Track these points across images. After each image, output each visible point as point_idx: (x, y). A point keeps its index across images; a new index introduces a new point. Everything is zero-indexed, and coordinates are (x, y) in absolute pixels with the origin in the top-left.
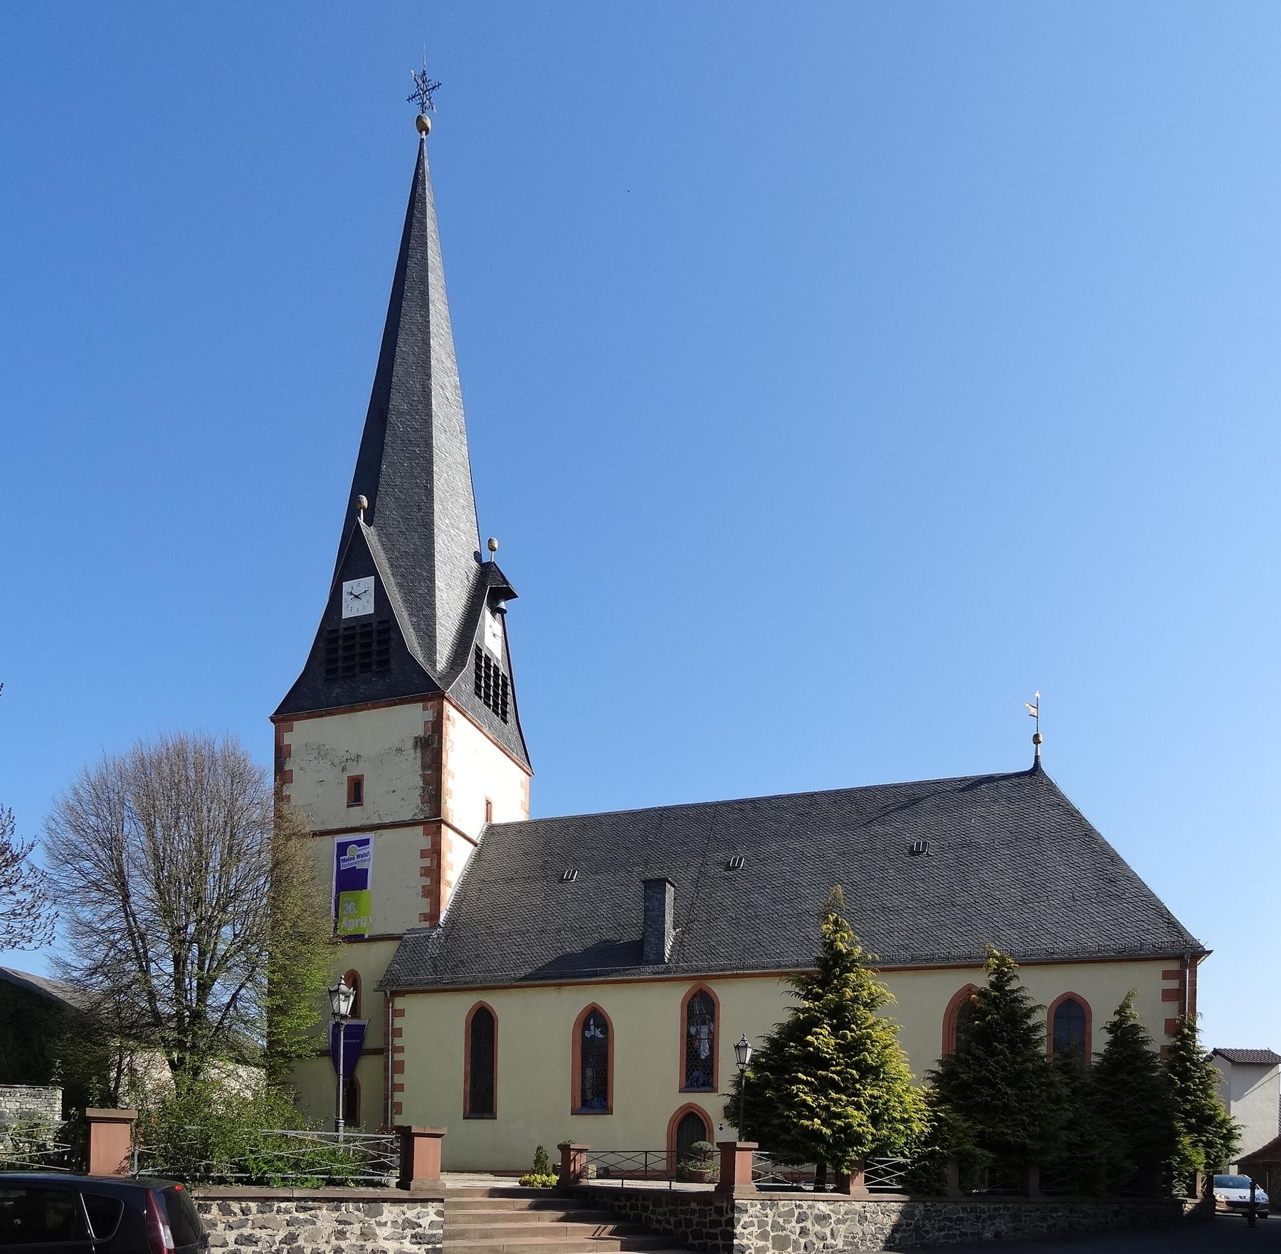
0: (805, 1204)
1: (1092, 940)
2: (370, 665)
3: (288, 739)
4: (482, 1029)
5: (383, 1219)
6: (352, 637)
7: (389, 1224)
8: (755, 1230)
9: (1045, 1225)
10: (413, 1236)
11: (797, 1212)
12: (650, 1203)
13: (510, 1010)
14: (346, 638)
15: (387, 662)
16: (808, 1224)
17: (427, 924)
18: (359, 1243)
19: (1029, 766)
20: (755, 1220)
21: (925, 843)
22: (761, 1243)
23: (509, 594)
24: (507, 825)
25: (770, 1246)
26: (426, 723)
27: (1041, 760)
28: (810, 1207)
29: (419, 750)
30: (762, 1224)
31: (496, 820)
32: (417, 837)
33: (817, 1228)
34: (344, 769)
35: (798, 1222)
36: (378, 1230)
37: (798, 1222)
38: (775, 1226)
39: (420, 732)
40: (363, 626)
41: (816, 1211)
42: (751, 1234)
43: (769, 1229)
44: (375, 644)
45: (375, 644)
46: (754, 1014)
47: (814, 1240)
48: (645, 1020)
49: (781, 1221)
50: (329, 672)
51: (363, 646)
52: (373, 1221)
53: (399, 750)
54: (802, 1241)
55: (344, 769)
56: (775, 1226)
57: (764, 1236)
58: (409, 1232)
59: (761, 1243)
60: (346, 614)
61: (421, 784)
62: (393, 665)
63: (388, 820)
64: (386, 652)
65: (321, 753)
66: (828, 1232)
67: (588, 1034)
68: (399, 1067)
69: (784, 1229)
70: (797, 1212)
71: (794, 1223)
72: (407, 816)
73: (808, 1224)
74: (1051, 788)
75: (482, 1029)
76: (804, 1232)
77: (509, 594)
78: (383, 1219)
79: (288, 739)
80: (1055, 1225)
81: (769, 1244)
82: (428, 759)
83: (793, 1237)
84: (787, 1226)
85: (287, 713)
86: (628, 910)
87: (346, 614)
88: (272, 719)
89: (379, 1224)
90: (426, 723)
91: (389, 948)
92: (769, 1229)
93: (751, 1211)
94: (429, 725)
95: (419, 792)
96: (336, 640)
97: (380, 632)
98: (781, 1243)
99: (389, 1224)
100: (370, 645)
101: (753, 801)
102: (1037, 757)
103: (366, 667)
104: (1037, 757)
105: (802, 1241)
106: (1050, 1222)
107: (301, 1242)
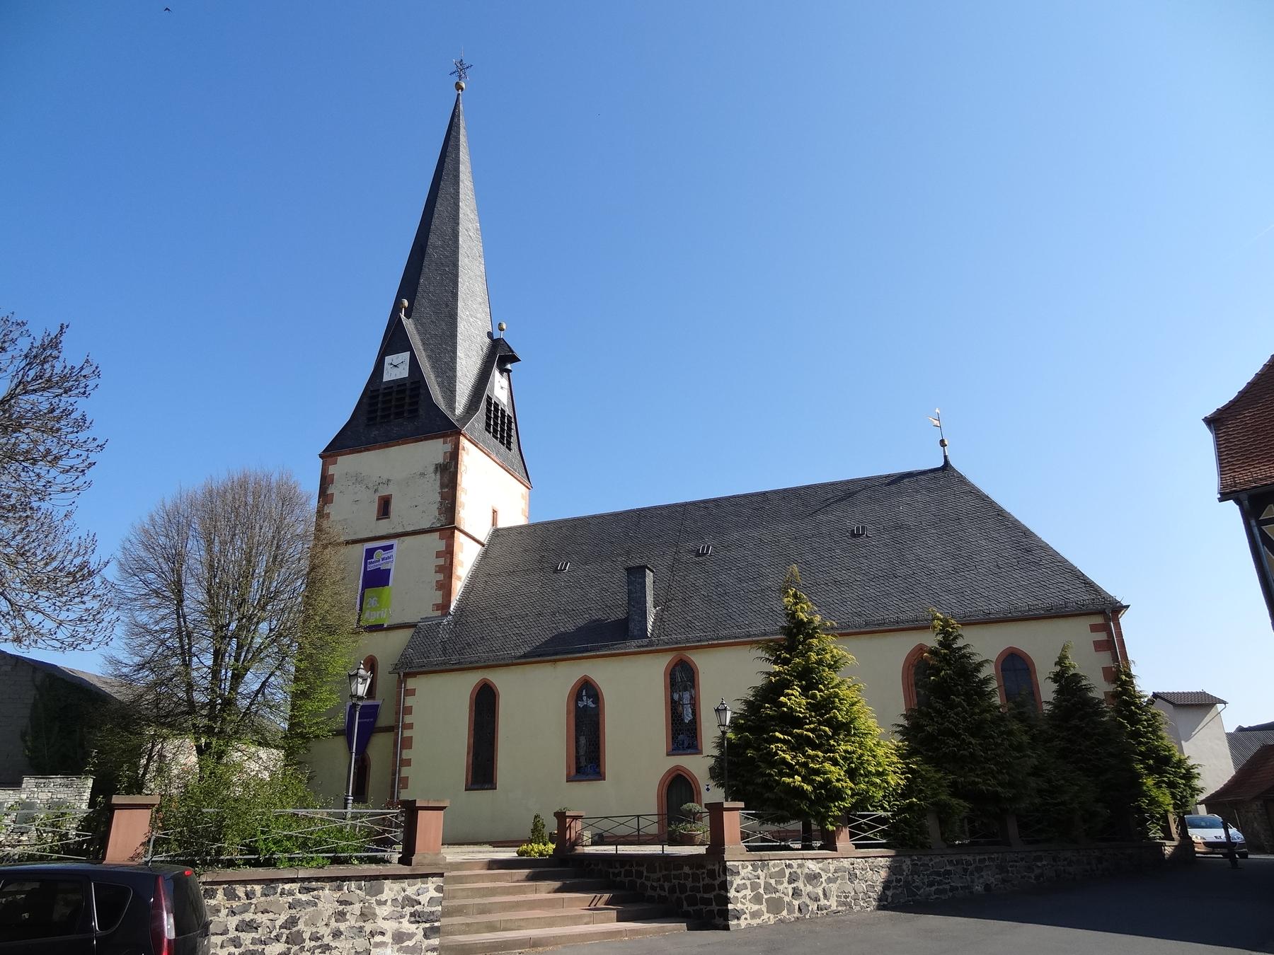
3: (332, 470)
5: (383, 897)
6: (390, 394)
7: (389, 903)
10: (412, 915)
11: (787, 871)
12: (644, 869)
14: (385, 395)
15: (416, 410)
16: (800, 884)
17: (439, 613)
18: (358, 925)
19: (940, 463)
20: (748, 883)
25: (765, 909)
27: (949, 459)
30: (755, 887)
31: (502, 524)
33: (809, 888)
35: (790, 883)
37: (790, 883)
38: (768, 888)
39: (441, 460)
41: (807, 871)
42: (744, 897)
43: (761, 891)
49: (773, 881)
52: (373, 900)
53: (423, 474)
54: (796, 903)
57: (757, 899)
58: (408, 910)
60: (386, 378)
62: (421, 412)
65: (358, 479)
67: (581, 704)
68: (407, 743)
69: (776, 891)
70: (787, 871)
71: (786, 884)
72: (426, 525)
73: (800, 884)
74: (962, 480)
76: (796, 893)
77: (514, 359)
78: (383, 897)
79: (332, 470)
83: (787, 899)
87: (386, 378)
88: (321, 456)
89: (380, 903)
91: (406, 634)
92: (761, 891)
93: (743, 872)
95: (436, 506)
97: (412, 390)
99: (389, 903)
100: (390, 401)
101: (715, 500)
105: (796, 903)
106: (1037, 871)
107: (301, 926)
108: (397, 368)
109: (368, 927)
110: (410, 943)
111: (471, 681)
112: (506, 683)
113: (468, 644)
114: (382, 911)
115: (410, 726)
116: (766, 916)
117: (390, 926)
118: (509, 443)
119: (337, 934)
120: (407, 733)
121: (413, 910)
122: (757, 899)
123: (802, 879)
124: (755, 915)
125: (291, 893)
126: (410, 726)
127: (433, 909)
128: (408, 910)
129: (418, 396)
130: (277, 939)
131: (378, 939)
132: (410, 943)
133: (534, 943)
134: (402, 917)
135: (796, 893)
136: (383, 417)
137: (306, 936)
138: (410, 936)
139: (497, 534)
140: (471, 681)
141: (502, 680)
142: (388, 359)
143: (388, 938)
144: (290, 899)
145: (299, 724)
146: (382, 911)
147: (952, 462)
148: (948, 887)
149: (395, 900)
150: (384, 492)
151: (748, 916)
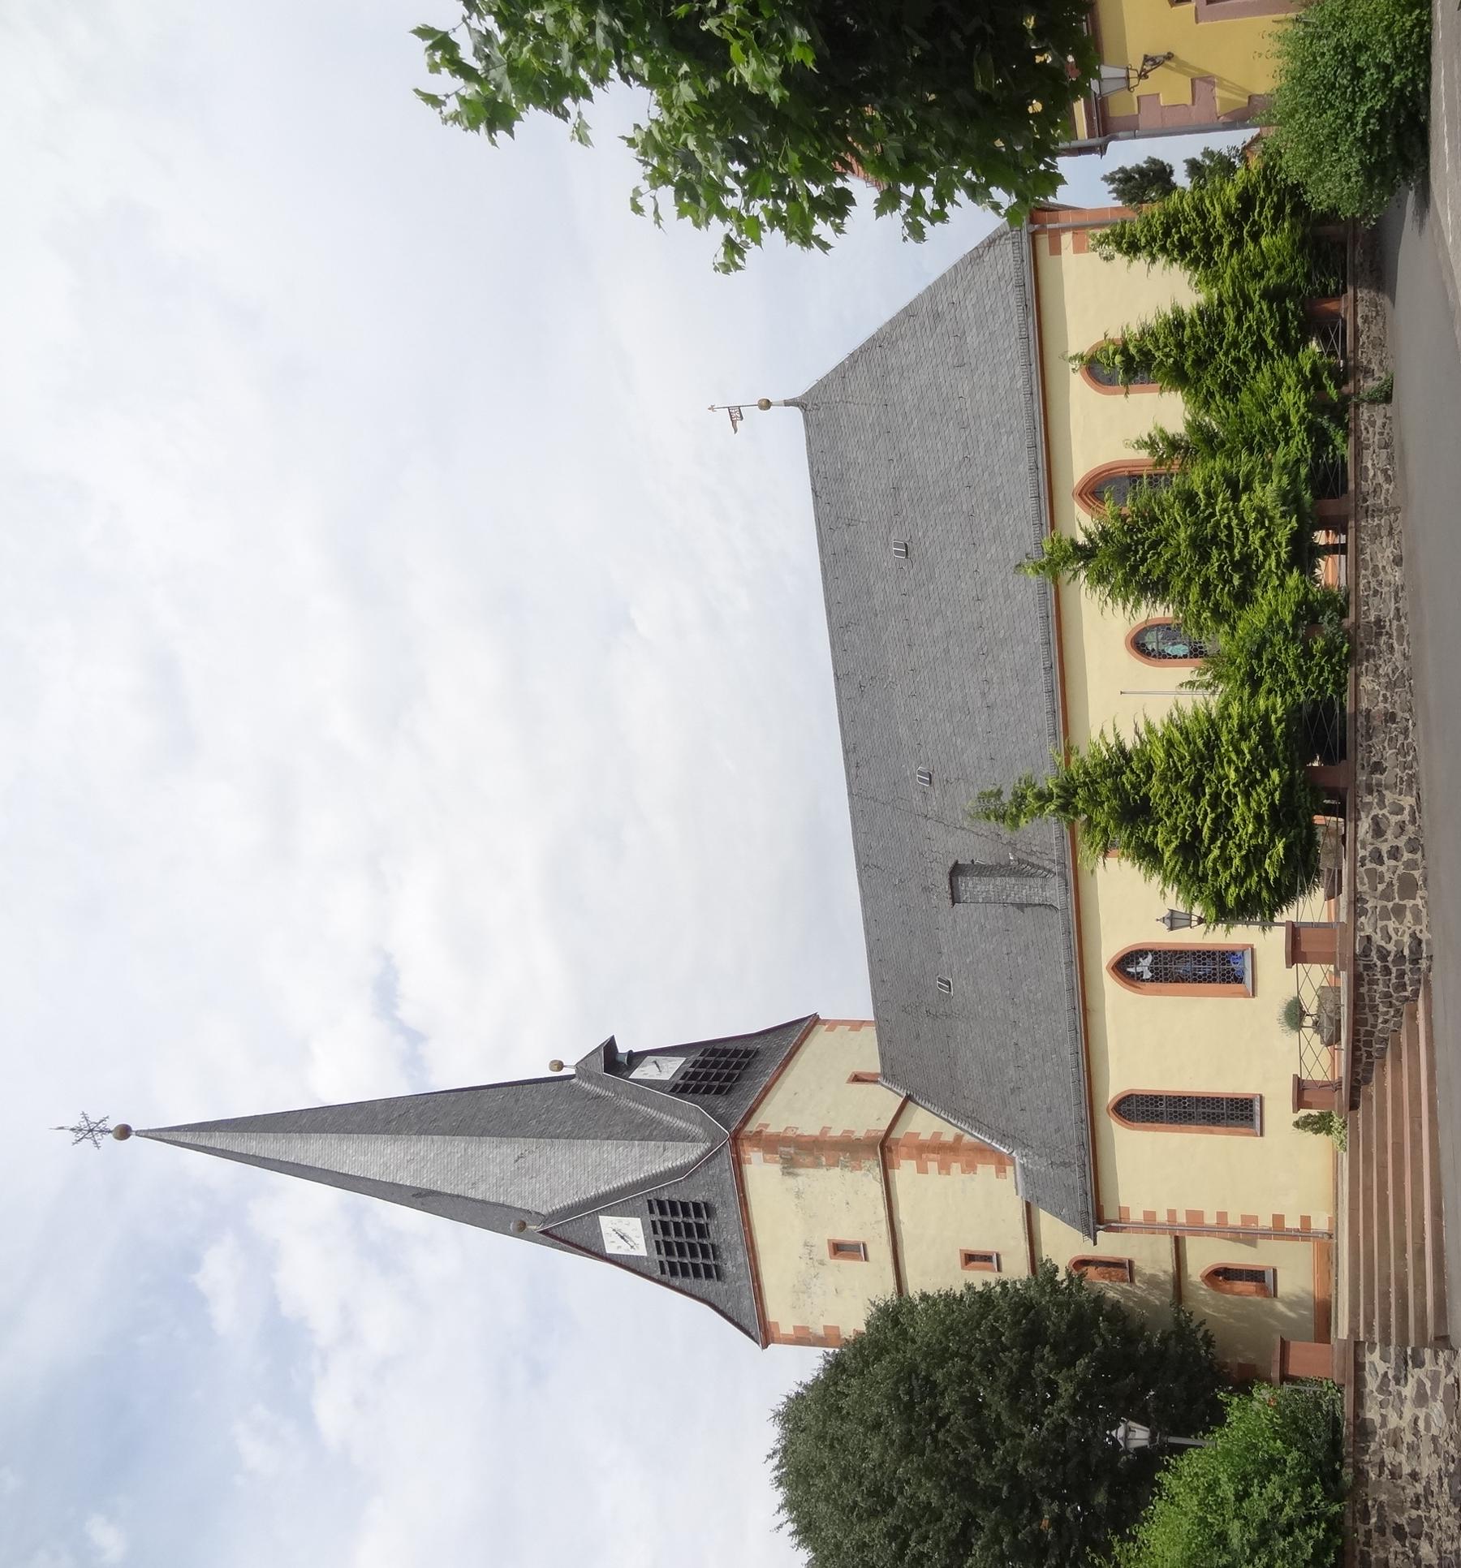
0: (1361, 853)
1: (1012, 349)
2: (700, 1227)
3: (786, 1328)
4: (1144, 1109)
5: (1378, 1420)
6: (668, 1245)
7: (1383, 1411)
8: (1392, 924)
9: (1386, 486)
10: (1398, 1383)
11: (1369, 865)
12: (1363, 1030)
13: (1121, 1077)
14: (669, 1252)
15: (696, 1205)
16: (1385, 848)
17: (1009, 1169)
18: (1405, 1451)
19: (796, 412)
20: (1380, 924)
21: (896, 545)
22: (1409, 916)
23: (610, 1047)
24: (883, 1056)
25: (1412, 902)
26: (765, 1161)
27: (788, 397)
28: (1364, 847)
29: (801, 1171)
30: (1385, 915)
31: (875, 1066)
32: (905, 1172)
33: (1389, 835)
34: (822, 1263)
35: (1382, 863)
36: (1391, 1425)
37: (1382, 863)
38: (1386, 896)
39: (776, 1168)
40: (655, 1232)
41: (1369, 836)
42: (1396, 931)
43: (1390, 905)
44: (676, 1219)
45: (676, 1219)
46: (1132, 903)
47: (1404, 838)
48: (1150, 1040)
49: (1380, 887)
50: (709, 1275)
51: (678, 1233)
52: (1380, 1432)
53: (798, 1195)
54: (1406, 856)
55: (822, 1263)
56: (1386, 896)
57: (1399, 912)
58: (1392, 1387)
59: (1409, 916)
60: (641, 1250)
61: (838, 1169)
62: (699, 1198)
63: (882, 1213)
64: (684, 1205)
65: (803, 1289)
66: (1394, 819)
67: (1148, 975)
68: (1195, 1216)
69: (1390, 884)
70: (1369, 865)
71: (1383, 869)
72: (878, 1189)
73: (1385, 848)
74: (823, 385)
75: (1144, 1109)
76: (1395, 853)
77: (610, 1047)
78: (1378, 1420)
79: (786, 1328)
80: (1385, 471)
81: (1409, 903)
82: (809, 1160)
83: (1401, 870)
84: (1387, 879)
85: (763, 1334)
86: (987, 918)
87: (641, 1250)
88: (765, 1346)
89: (1384, 1424)
90: (765, 1161)
91: (1047, 1222)
92: (1390, 905)
93: (1369, 931)
94: (768, 1157)
95: (848, 1174)
96: (672, 1265)
97: (663, 1212)
98: (1408, 887)
99: (1383, 1411)
100: (676, 1225)
101: (846, 752)
102: (787, 403)
103: (702, 1231)
104: (787, 403)
105: (1406, 856)
106: (1380, 479)
107: (1402, 1520)
108: (626, 1233)
109: (1408, 1437)
110: (1428, 1385)
111: (1112, 993)
112: (1121, 1077)
113: (1057, 1131)
114: (1393, 1421)
115: (1172, 1213)
116: (1419, 902)
117: (1408, 1411)
118: (747, 1053)
119: (1414, 1476)
120: (1182, 1219)
121: (1392, 1383)
122: (1399, 912)
123: (1378, 845)
124: (1417, 919)
125: (1368, 1533)
126: (1172, 1213)
127: (1393, 1357)
128: (1392, 1387)
129: (672, 1204)
130: (1416, 1550)
131: (1421, 1424)
132: (1428, 1385)
133: (1437, 1212)
134: (1400, 1394)
135: (1395, 853)
136: (705, 1255)
137: (1414, 1513)
138: (1420, 1384)
139: (890, 1074)
140: (1112, 993)
141: (1110, 945)
142: (610, 1249)
143: (1422, 1413)
144: (1375, 1535)
145: (1178, 366)
146: (1393, 1421)
147: (798, 391)
148: (1395, 623)
149: (1381, 1405)
150: (825, 1251)
151: (1418, 928)
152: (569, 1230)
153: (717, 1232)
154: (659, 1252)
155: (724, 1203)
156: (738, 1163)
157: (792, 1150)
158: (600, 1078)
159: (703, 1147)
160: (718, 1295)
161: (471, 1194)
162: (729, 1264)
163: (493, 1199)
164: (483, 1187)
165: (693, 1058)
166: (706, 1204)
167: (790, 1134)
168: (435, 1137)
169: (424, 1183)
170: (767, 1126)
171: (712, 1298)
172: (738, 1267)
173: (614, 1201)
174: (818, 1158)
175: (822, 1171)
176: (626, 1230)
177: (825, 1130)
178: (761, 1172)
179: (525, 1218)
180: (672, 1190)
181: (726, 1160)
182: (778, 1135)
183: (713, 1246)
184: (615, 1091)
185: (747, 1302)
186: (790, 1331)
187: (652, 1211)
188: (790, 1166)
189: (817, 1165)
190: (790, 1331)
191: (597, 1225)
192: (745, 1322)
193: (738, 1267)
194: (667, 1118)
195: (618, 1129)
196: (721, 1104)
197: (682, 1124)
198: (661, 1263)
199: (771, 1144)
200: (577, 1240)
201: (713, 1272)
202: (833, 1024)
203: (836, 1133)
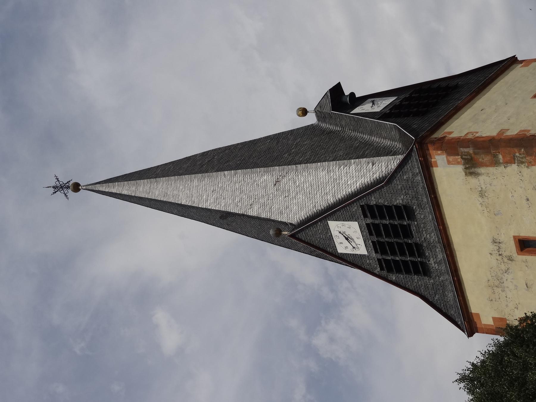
23: (337, 90)
26: (449, 163)
29: (482, 170)
34: (510, 259)
40: (371, 234)
44: (384, 222)
45: (384, 222)
50: (417, 272)
53: (482, 194)
55: (510, 259)
60: (362, 250)
61: (514, 166)
65: (497, 284)
82: (487, 159)
87: (362, 250)
88: (470, 334)
90: (449, 163)
94: (451, 158)
95: (526, 171)
103: (407, 232)
108: (349, 236)
150: (511, 248)
152: (308, 236)
153: (418, 232)
154: (376, 252)
155: (420, 205)
156: (427, 168)
157: (471, 150)
158: (331, 116)
159: (401, 157)
160: (426, 288)
161: (250, 213)
162: (432, 261)
163: (263, 216)
164: (256, 207)
165: (402, 97)
166: (405, 206)
167: (470, 136)
168: (226, 172)
169: (221, 207)
170: (450, 133)
171: (422, 291)
172: (439, 263)
173: (338, 209)
174: (495, 156)
175: (501, 169)
176: (349, 232)
177: (502, 132)
178: (448, 174)
179: (282, 227)
180: (377, 195)
181: (415, 165)
182: (459, 138)
183: (417, 244)
184: (342, 126)
185: (451, 295)
186: (490, 322)
187: (365, 216)
188: (471, 166)
189: (495, 163)
190: (490, 322)
191: (328, 229)
192: (452, 312)
193: (439, 263)
194: (375, 139)
195: (341, 153)
196: (416, 123)
197: (388, 143)
198: (379, 260)
199: (452, 147)
200: (316, 243)
201: (423, 270)
202: (527, 63)
203: (513, 132)
